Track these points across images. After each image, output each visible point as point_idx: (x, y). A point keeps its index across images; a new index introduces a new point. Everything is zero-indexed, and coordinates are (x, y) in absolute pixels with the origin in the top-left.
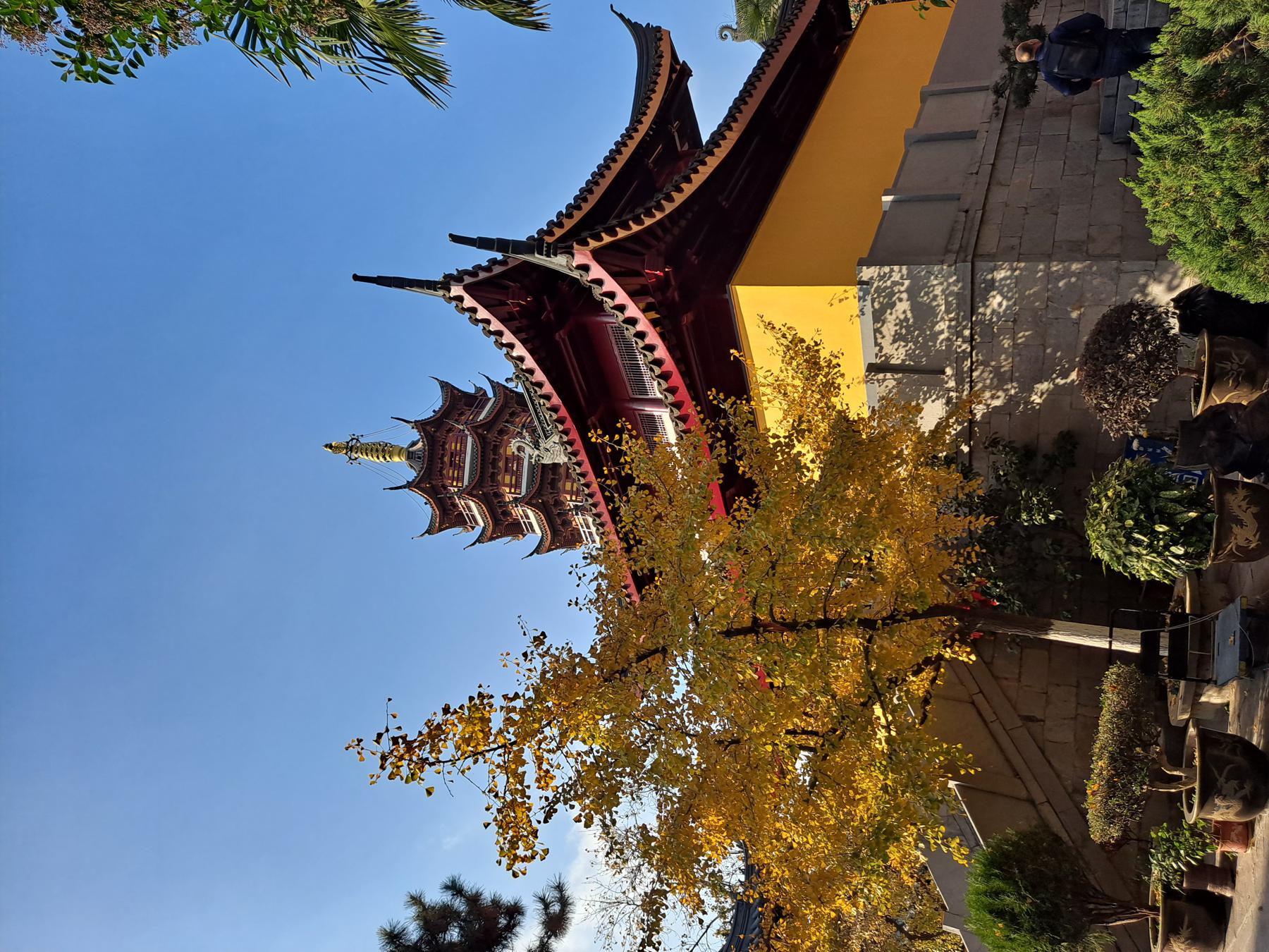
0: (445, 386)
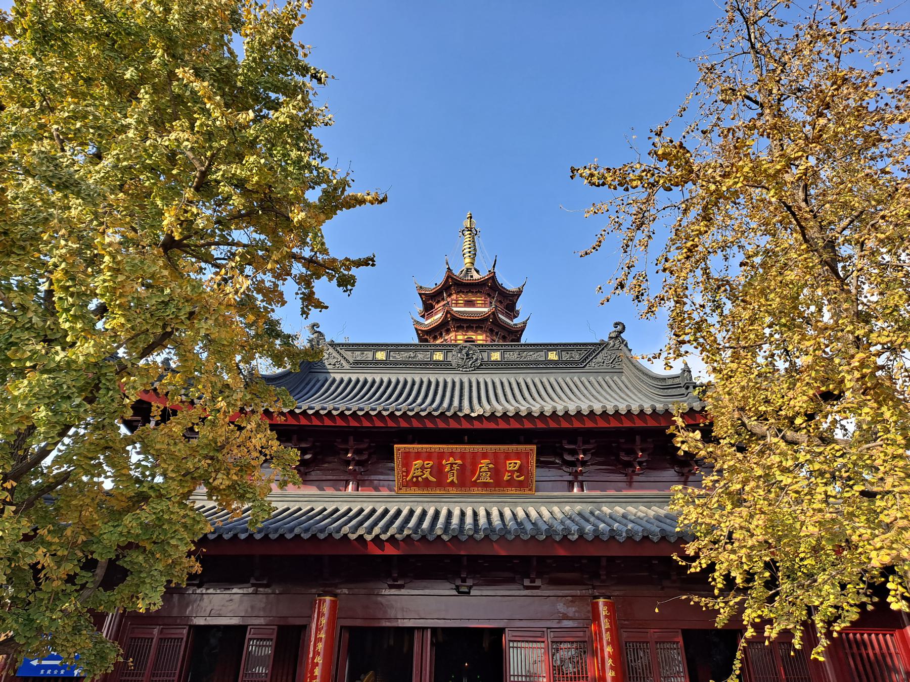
0: (518, 294)
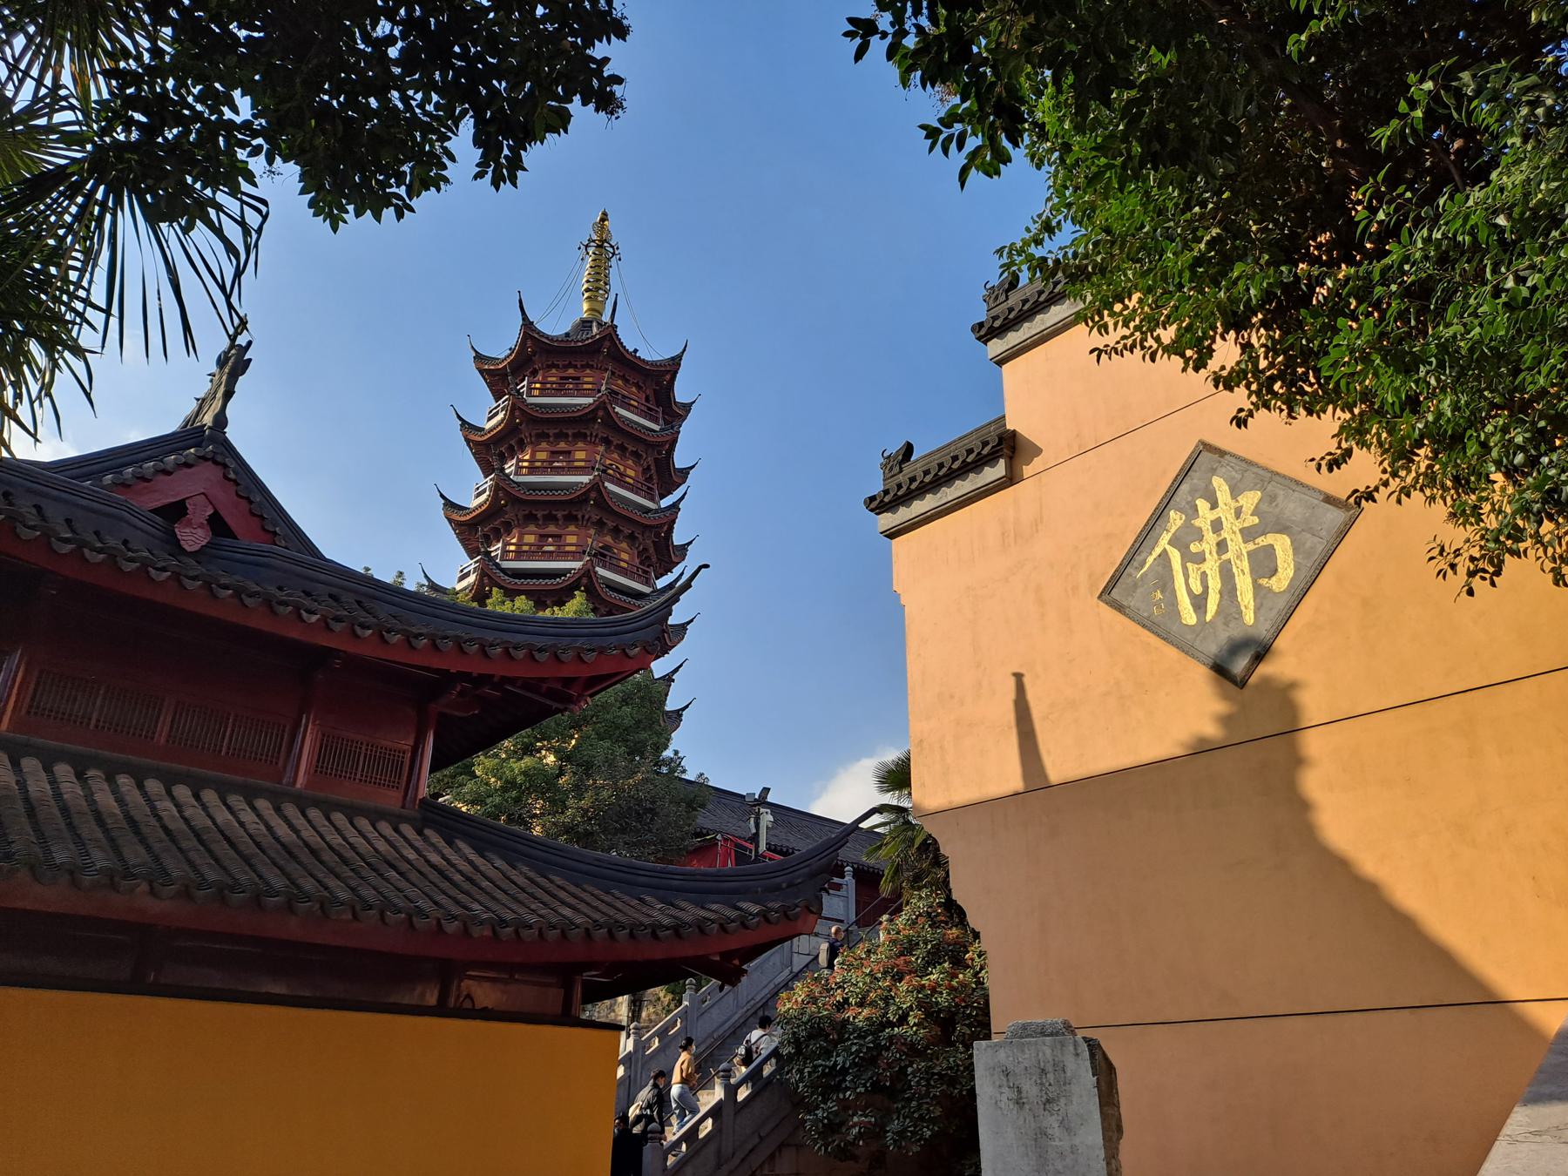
0: (676, 362)
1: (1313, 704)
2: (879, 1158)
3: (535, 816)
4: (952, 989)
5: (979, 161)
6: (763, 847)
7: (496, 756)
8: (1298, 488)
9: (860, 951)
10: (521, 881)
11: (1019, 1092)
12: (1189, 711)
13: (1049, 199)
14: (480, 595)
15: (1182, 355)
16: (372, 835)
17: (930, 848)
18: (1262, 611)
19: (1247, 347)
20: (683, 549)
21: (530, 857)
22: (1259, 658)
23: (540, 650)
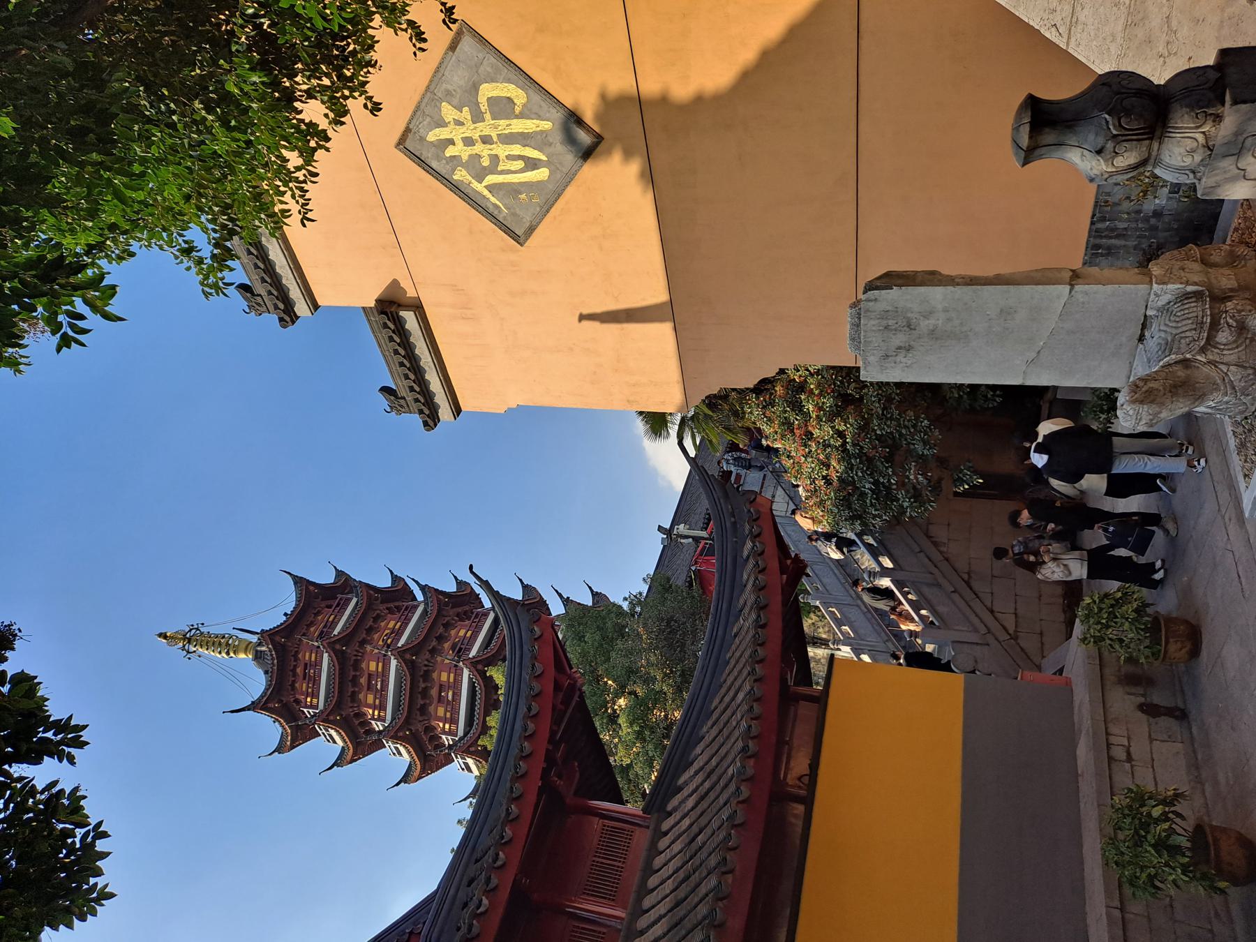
0: (299, 581)
1: (620, 83)
2: (942, 462)
3: (666, 716)
4: (820, 395)
5: (99, 303)
6: (704, 534)
7: (616, 746)
8: (442, 70)
9: (788, 463)
10: (714, 732)
11: (900, 348)
12: (617, 181)
13: (161, 248)
14: (482, 755)
15: (314, 150)
16: (668, 854)
17: (713, 402)
18: (541, 114)
19: (310, 94)
20: (460, 583)
21: (705, 698)
22: (579, 122)
23: (529, 709)
